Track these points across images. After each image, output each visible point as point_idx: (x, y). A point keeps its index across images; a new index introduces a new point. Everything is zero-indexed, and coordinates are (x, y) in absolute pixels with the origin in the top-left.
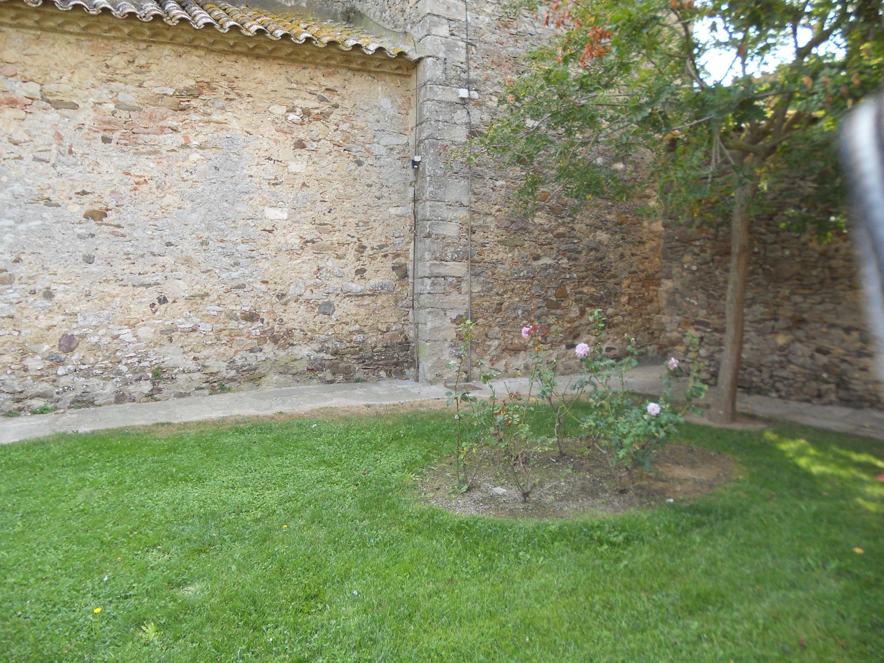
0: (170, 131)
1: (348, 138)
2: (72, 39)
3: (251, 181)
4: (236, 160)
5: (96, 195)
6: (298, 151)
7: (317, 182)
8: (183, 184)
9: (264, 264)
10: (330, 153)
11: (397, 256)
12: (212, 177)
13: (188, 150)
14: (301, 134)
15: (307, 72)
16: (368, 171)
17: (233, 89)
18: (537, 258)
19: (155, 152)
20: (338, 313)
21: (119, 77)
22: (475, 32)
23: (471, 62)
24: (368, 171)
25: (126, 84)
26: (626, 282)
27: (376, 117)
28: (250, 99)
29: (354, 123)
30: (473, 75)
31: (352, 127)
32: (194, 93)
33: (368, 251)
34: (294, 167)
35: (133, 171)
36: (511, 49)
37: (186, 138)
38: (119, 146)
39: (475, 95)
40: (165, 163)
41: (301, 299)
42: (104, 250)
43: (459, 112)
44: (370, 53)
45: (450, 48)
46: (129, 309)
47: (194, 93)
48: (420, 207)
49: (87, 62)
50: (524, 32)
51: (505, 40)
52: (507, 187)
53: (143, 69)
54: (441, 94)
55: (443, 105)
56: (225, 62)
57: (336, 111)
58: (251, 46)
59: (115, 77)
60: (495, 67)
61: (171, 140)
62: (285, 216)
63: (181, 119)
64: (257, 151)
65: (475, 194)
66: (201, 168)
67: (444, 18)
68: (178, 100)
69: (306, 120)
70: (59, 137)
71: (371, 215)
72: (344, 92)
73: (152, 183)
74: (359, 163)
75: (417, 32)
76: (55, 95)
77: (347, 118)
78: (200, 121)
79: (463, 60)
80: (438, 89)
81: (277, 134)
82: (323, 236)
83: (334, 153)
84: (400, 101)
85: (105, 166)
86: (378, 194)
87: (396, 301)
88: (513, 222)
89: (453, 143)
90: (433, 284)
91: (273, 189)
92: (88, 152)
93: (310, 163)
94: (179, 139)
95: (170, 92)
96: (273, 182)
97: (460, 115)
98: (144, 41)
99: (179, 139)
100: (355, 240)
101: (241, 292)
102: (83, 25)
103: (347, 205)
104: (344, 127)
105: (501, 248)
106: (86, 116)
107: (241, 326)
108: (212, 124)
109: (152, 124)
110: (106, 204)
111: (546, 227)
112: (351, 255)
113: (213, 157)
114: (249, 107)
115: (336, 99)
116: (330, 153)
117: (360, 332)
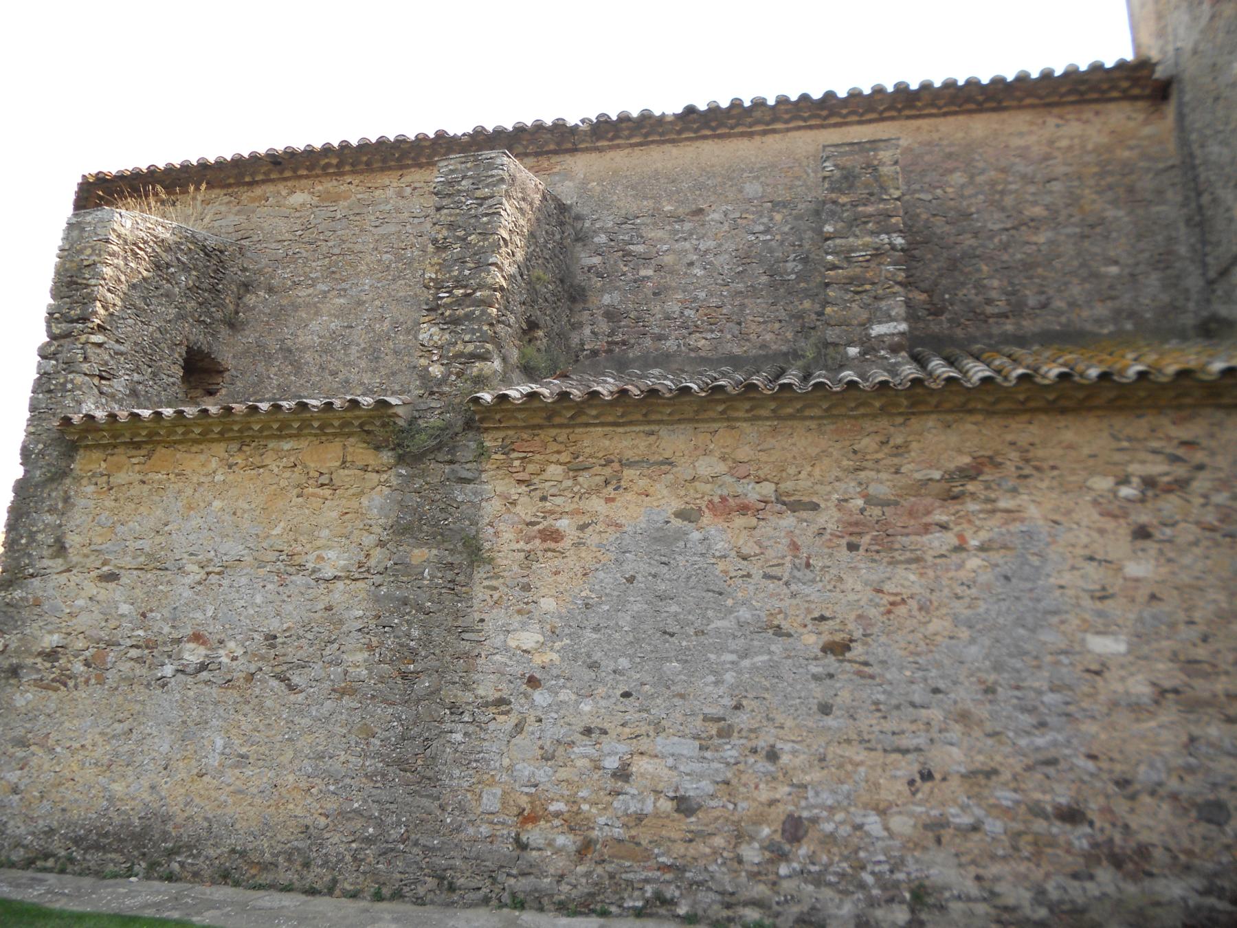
0: (938, 528)
2: (813, 424)
5: (838, 621)
8: (957, 604)
10: (1196, 543)
12: (1000, 590)
13: (964, 555)
14: (1144, 519)
19: (918, 560)
21: (869, 464)
25: (878, 471)
28: (1055, 473)
32: (969, 474)
34: (1134, 569)
35: (887, 587)
37: (961, 537)
40: (931, 573)
42: (845, 696)
46: (877, 786)
47: (969, 474)
53: (900, 450)
56: (1014, 426)
59: (865, 464)
61: (939, 542)
62: (1122, 648)
63: (953, 511)
66: (984, 578)
68: (946, 486)
70: (795, 547)
72: (1213, 444)
78: (981, 511)
91: (1099, 605)
94: (950, 539)
95: (937, 475)
96: (1098, 594)
98: (901, 414)
99: (950, 539)
101: (1051, 770)
106: (828, 518)
107: (1055, 830)
108: (999, 515)
109: (912, 522)
113: (1001, 562)
115: (1199, 457)
116: (1196, 543)
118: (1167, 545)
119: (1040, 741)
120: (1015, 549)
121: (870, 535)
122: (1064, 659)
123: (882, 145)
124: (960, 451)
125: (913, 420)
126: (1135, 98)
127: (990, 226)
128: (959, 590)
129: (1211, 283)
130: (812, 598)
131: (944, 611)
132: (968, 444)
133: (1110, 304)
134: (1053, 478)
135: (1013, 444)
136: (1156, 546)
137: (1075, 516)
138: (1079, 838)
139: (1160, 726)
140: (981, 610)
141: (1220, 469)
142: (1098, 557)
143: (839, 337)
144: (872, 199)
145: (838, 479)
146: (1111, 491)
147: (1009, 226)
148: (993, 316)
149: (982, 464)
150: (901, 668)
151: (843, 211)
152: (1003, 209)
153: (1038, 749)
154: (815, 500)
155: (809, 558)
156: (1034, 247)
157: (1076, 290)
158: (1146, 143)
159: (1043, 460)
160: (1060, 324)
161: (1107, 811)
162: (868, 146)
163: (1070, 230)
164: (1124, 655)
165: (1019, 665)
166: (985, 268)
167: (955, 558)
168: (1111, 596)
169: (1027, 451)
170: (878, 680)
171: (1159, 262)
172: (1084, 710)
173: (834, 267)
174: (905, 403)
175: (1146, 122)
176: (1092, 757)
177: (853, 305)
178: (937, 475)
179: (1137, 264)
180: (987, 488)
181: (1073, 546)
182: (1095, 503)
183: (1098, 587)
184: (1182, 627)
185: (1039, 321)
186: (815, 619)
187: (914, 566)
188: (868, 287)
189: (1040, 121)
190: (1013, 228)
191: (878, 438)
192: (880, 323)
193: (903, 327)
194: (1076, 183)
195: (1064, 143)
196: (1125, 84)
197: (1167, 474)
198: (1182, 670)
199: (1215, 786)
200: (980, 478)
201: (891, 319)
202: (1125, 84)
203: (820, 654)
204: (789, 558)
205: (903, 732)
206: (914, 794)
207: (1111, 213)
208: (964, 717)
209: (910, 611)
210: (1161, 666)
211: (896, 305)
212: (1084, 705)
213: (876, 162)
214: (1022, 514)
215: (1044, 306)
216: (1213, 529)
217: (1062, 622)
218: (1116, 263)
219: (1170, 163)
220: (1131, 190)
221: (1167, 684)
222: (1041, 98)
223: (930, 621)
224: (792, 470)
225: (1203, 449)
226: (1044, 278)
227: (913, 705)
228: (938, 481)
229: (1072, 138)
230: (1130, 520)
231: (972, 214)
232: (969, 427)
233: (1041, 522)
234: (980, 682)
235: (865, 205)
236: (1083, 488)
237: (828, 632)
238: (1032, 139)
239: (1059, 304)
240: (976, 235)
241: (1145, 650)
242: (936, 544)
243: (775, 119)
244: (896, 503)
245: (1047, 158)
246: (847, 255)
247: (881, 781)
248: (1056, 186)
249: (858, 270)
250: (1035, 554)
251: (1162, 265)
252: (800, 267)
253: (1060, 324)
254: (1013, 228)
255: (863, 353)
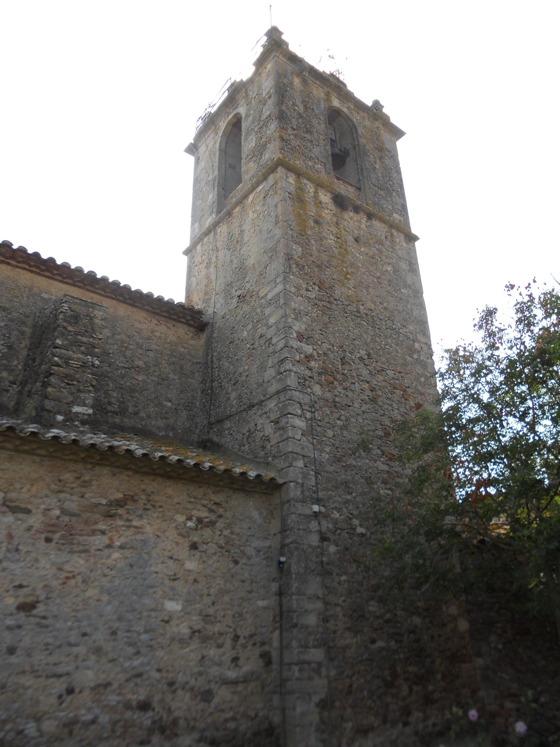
0: (100, 533)
1: (228, 542)
2: (37, 459)
3: (156, 577)
4: (147, 558)
5: (30, 588)
6: (193, 552)
7: (204, 579)
8: (104, 579)
9: (160, 653)
10: (215, 554)
11: (263, 644)
12: (126, 573)
13: (111, 550)
14: (196, 538)
15: (202, 490)
16: (242, 569)
17: (149, 501)
18: (373, 641)
19: (86, 551)
20: (216, 700)
21: (67, 489)
22: (320, 464)
23: (319, 486)
24: (242, 569)
25: (72, 495)
26: (438, 661)
27: (249, 525)
28: (161, 510)
29: (233, 530)
30: (321, 494)
31: (232, 533)
32: (120, 504)
33: (242, 641)
34: (190, 565)
35: (67, 567)
36: (343, 476)
37: (111, 539)
38: (58, 545)
39: (323, 509)
40: (92, 560)
41: (188, 687)
42: (27, 641)
43: (313, 522)
44: (252, 478)
45: (305, 476)
46: (38, 702)
47: (120, 504)
48: (285, 600)
49: (45, 477)
50: (350, 464)
51: (339, 470)
52: (349, 581)
53: (86, 484)
54: (301, 509)
55: (302, 517)
56: (146, 481)
57: (221, 520)
58: (168, 470)
59: (65, 489)
60: (334, 489)
61: (99, 541)
62: (179, 608)
63: (109, 524)
64: (162, 551)
65: (327, 588)
66: (120, 565)
67: (300, 455)
68: (108, 509)
69: (199, 526)
70: (10, 536)
71: (245, 607)
72: (227, 506)
73: (79, 578)
74: (236, 562)
75: (280, 463)
76: (15, 502)
77: (228, 526)
78: (123, 526)
79: (314, 484)
80: (299, 505)
81: (179, 537)
82: (209, 627)
83: (218, 554)
84: (265, 513)
85: (43, 562)
86: (249, 589)
87: (263, 687)
88: (354, 611)
89: (310, 546)
90: (301, 670)
91: (172, 584)
92: (31, 550)
93: (201, 562)
94: (105, 540)
95: (104, 502)
96: (172, 577)
97: (314, 525)
98: (91, 463)
99: (105, 540)
100: (231, 630)
101: (138, 680)
102: (51, 450)
103: (226, 598)
104: (226, 532)
105: (348, 634)
106: (36, 520)
107: (135, 716)
108: (132, 529)
109: (86, 528)
110: (38, 596)
111: (378, 614)
112: (229, 643)
113: (129, 556)
114: (160, 515)
115: (221, 511)
116: (215, 554)
117: (234, 719)
118: (204, 553)
119: (136, 663)
120: (137, 549)
121: (61, 533)
122: (153, 614)
123: (97, 307)
124: (118, 490)
125: (97, 468)
126: (191, 325)
127: (117, 363)
128: (106, 571)
129: (210, 424)
130: (16, 572)
131: (96, 584)
132: (122, 487)
133: (164, 421)
134: (160, 512)
135: (144, 490)
136: (199, 554)
137: (167, 534)
138: (146, 719)
139: (191, 651)
140: (116, 584)
141: (228, 519)
142: (175, 557)
143: (53, 407)
144: (86, 334)
145: (46, 496)
146: (183, 522)
147: (126, 366)
148: (111, 412)
149: (127, 499)
150: (66, 620)
151: (69, 335)
152: (125, 357)
153: (134, 668)
154: (29, 507)
155: (19, 544)
156: (136, 382)
157: (151, 409)
158: (191, 347)
159: (157, 502)
160: (141, 425)
161: (162, 701)
162: (90, 304)
163: (153, 378)
164: (181, 611)
165: (131, 618)
166: (111, 385)
167: (106, 551)
168: (178, 579)
169: (150, 496)
170: (50, 629)
171: (187, 406)
172: (159, 643)
173: (58, 365)
174: (98, 458)
175: (192, 338)
176: (159, 670)
177: (64, 390)
178: (104, 502)
179: (179, 405)
180: (128, 513)
181: (165, 550)
182: (176, 528)
183: (172, 573)
184: (205, 597)
185: (132, 420)
186: (15, 587)
187: (83, 555)
188: (75, 383)
189: (149, 319)
190: (128, 368)
191: (75, 475)
192: (78, 405)
193: (90, 411)
194: (160, 356)
195: (158, 334)
196: (189, 318)
197: (207, 518)
198: (203, 620)
199: (209, 681)
200: (126, 507)
201: (85, 405)
202: (189, 318)
203: (15, 612)
204: (5, 544)
205: (60, 663)
206: (61, 704)
207: (171, 376)
208: (98, 651)
209: (77, 583)
210: (194, 618)
211: (89, 398)
212: (159, 640)
213: (92, 315)
214: (143, 530)
215: (136, 414)
216: (222, 548)
217: (155, 592)
218: (170, 401)
219: (199, 361)
220: (181, 368)
221: (196, 628)
222: (153, 308)
223: (87, 590)
224: (18, 486)
225: (223, 508)
226: (138, 399)
227: (70, 645)
228: (104, 505)
229: (161, 333)
230: (190, 539)
231: (110, 354)
232: (124, 477)
233: (151, 535)
234: (110, 628)
235: (82, 336)
236: (172, 519)
237: (23, 597)
238: (145, 326)
239: (143, 414)
240: (110, 365)
241: (189, 609)
242: (97, 542)
243: (12, 258)
244: (78, 515)
245: (149, 338)
246: (67, 361)
247: (41, 698)
248: (151, 354)
249: (72, 372)
250: (146, 553)
251: (189, 408)
252: (5, 350)
253: (141, 425)
254: (128, 368)
255: (65, 421)
